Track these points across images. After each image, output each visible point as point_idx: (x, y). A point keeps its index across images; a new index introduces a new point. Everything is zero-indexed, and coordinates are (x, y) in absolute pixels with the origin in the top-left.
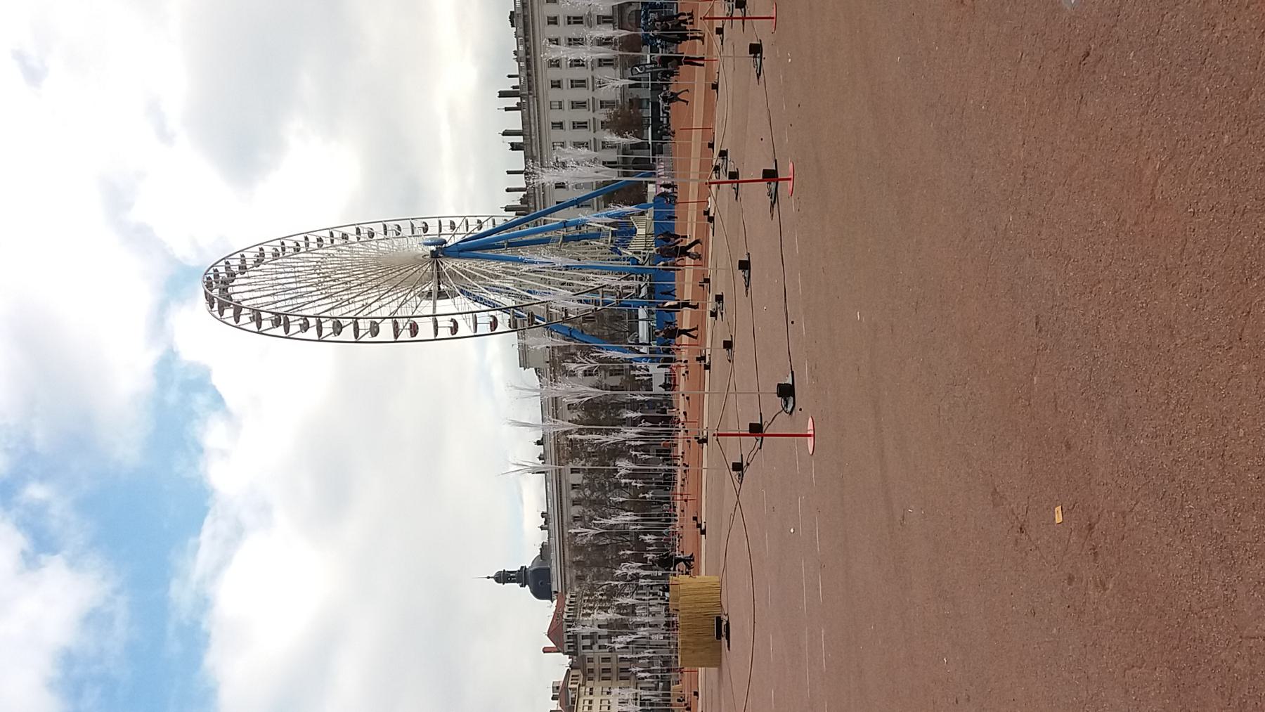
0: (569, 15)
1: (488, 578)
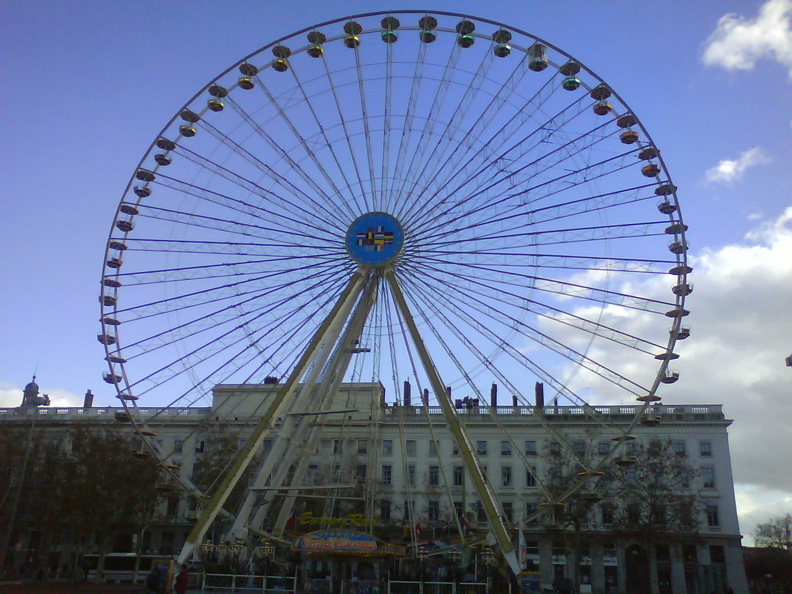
0: (536, 469)
1: (34, 377)
